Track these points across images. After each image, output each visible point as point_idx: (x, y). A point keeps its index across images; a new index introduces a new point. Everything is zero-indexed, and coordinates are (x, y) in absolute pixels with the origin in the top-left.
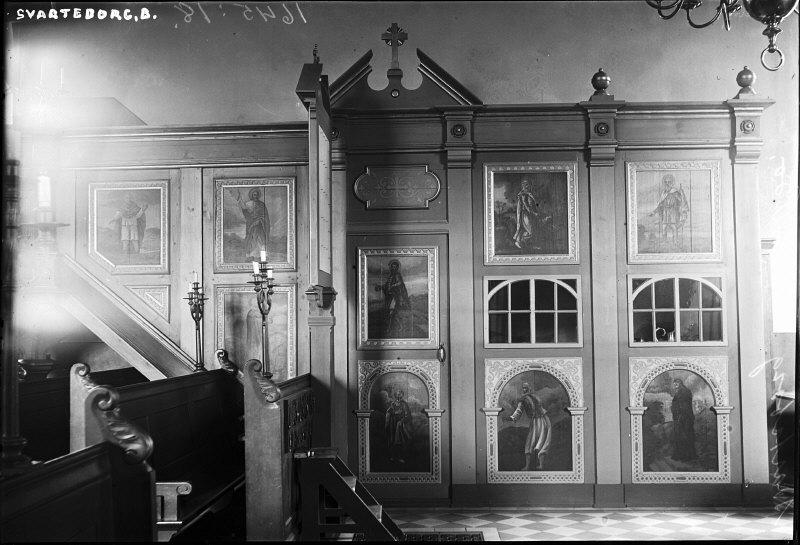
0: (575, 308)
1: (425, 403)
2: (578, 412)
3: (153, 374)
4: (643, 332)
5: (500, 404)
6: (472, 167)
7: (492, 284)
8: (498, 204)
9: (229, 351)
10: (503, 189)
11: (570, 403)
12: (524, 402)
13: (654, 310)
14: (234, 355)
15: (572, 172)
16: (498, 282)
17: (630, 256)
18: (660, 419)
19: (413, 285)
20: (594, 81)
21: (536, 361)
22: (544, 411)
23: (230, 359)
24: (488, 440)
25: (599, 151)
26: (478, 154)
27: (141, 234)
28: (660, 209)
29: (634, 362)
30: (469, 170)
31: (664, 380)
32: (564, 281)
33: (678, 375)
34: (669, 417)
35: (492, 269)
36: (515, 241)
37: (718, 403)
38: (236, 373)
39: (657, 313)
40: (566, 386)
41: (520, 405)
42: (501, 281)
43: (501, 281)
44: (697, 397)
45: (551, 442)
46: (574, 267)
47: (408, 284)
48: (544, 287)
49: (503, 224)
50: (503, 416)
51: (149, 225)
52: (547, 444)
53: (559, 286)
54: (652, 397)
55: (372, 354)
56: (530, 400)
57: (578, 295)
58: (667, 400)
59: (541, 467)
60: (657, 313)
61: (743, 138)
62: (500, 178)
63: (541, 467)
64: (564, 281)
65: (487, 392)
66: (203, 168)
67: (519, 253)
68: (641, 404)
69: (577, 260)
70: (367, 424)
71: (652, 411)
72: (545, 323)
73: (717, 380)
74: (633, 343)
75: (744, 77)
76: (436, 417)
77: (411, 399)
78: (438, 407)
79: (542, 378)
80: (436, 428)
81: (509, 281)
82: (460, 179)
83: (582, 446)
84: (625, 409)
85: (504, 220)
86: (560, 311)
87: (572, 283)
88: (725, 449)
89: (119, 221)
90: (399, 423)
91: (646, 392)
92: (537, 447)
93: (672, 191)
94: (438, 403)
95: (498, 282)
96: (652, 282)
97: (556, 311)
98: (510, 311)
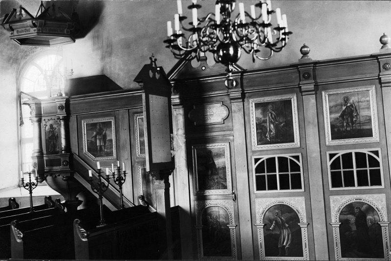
0: (379, 166)
1: (228, 221)
2: (385, 225)
3: (113, 208)
4: (336, 183)
5: (263, 222)
6: (316, 94)
7: (331, 156)
8: (257, 119)
9: (145, 196)
10: (260, 111)
11: (299, 221)
12: (276, 221)
13: (342, 170)
14: (147, 198)
15: (372, 90)
16: (259, 159)
17: (228, 147)
18: (349, 229)
19: (219, 162)
20: (381, 40)
21: (358, 196)
22: (287, 225)
23: (145, 199)
24: (259, 240)
25: (385, 78)
26: (319, 86)
27: (105, 143)
28: (342, 116)
29: (332, 199)
30: (314, 95)
31: (349, 208)
32: (371, 152)
33: (357, 205)
34: (354, 228)
35: (330, 147)
36: (267, 137)
37: (381, 220)
38: (148, 206)
39: (291, 174)
40: (297, 212)
41: (274, 222)
42: (337, 154)
43: (337, 154)
44: (369, 217)
45: (291, 242)
46: (377, 144)
47: (216, 162)
48: (360, 157)
49: (261, 129)
50: (266, 227)
51: (108, 138)
52: (289, 243)
53: (290, 160)
54: (345, 217)
55: (201, 198)
56: (280, 220)
57: (380, 160)
58: (352, 218)
59: (287, 254)
60: (291, 174)
61: (304, 82)
62: (257, 106)
63: (287, 254)
64: (371, 152)
65: (332, 213)
66: (129, 110)
67: (270, 143)
68: (338, 221)
69: (378, 139)
70: (201, 231)
71: (344, 225)
72: (284, 179)
73: (380, 207)
74: (303, 190)
75: (303, 49)
76: (233, 229)
77: (221, 220)
78: (234, 224)
79: (284, 209)
80: (233, 233)
81: (341, 153)
82: (236, 106)
83: (307, 243)
84: (328, 224)
85: (260, 126)
86: (339, 170)
87: (297, 158)
88: (387, 246)
89: (95, 137)
90: (216, 232)
91: (340, 214)
92: (285, 244)
93: (349, 105)
94: (234, 221)
95: (259, 159)
96: (340, 155)
97: (368, 169)
98: (355, 170)
